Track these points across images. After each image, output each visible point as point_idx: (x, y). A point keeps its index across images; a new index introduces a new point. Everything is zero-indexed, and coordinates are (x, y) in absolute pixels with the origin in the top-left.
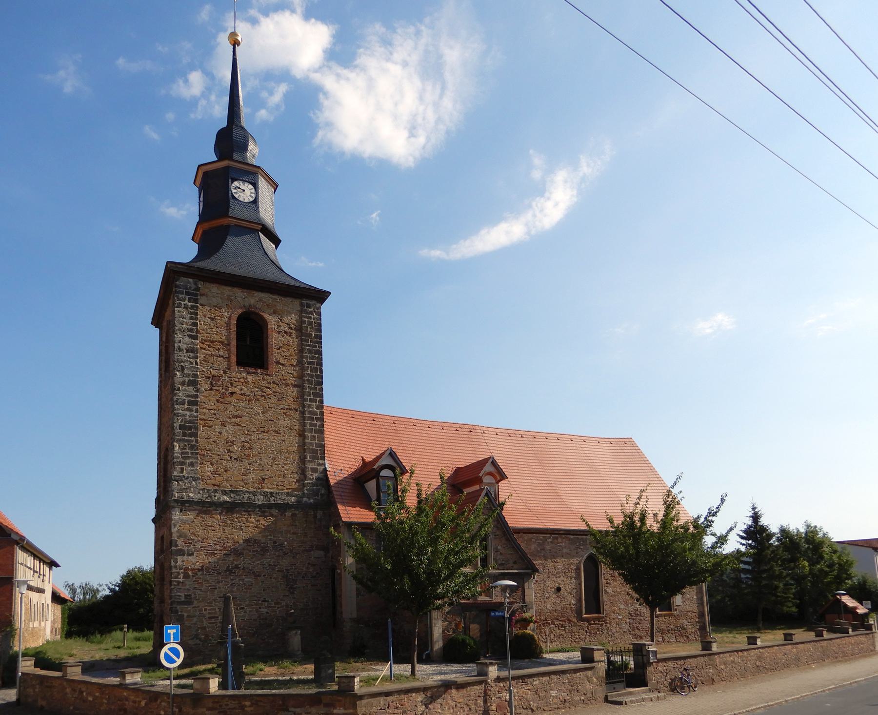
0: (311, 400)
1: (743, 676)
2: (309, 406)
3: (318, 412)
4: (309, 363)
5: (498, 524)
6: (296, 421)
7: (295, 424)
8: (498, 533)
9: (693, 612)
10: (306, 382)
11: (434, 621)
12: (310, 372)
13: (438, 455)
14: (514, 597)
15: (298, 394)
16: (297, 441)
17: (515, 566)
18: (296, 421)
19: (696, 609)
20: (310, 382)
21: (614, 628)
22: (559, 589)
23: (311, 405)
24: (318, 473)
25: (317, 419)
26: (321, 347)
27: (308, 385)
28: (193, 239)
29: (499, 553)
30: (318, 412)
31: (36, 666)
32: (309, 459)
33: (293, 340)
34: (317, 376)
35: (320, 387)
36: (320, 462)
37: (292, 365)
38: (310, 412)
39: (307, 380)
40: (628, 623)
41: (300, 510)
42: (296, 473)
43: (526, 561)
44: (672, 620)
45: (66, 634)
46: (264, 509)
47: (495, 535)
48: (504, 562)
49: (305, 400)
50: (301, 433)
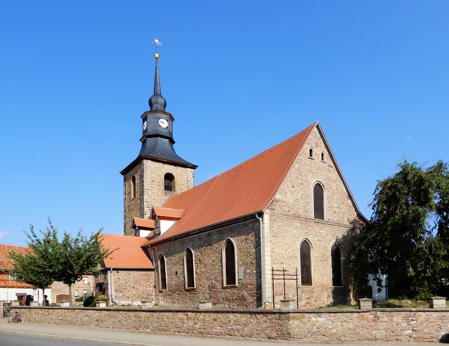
1: (49, 323)
9: (252, 285)
13: (190, 197)
19: (255, 283)
21: (201, 296)
22: (177, 273)
28: (140, 140)
31: (359, 300)
40: (208, 293)
44: (235, 291)
45: (373, 279)
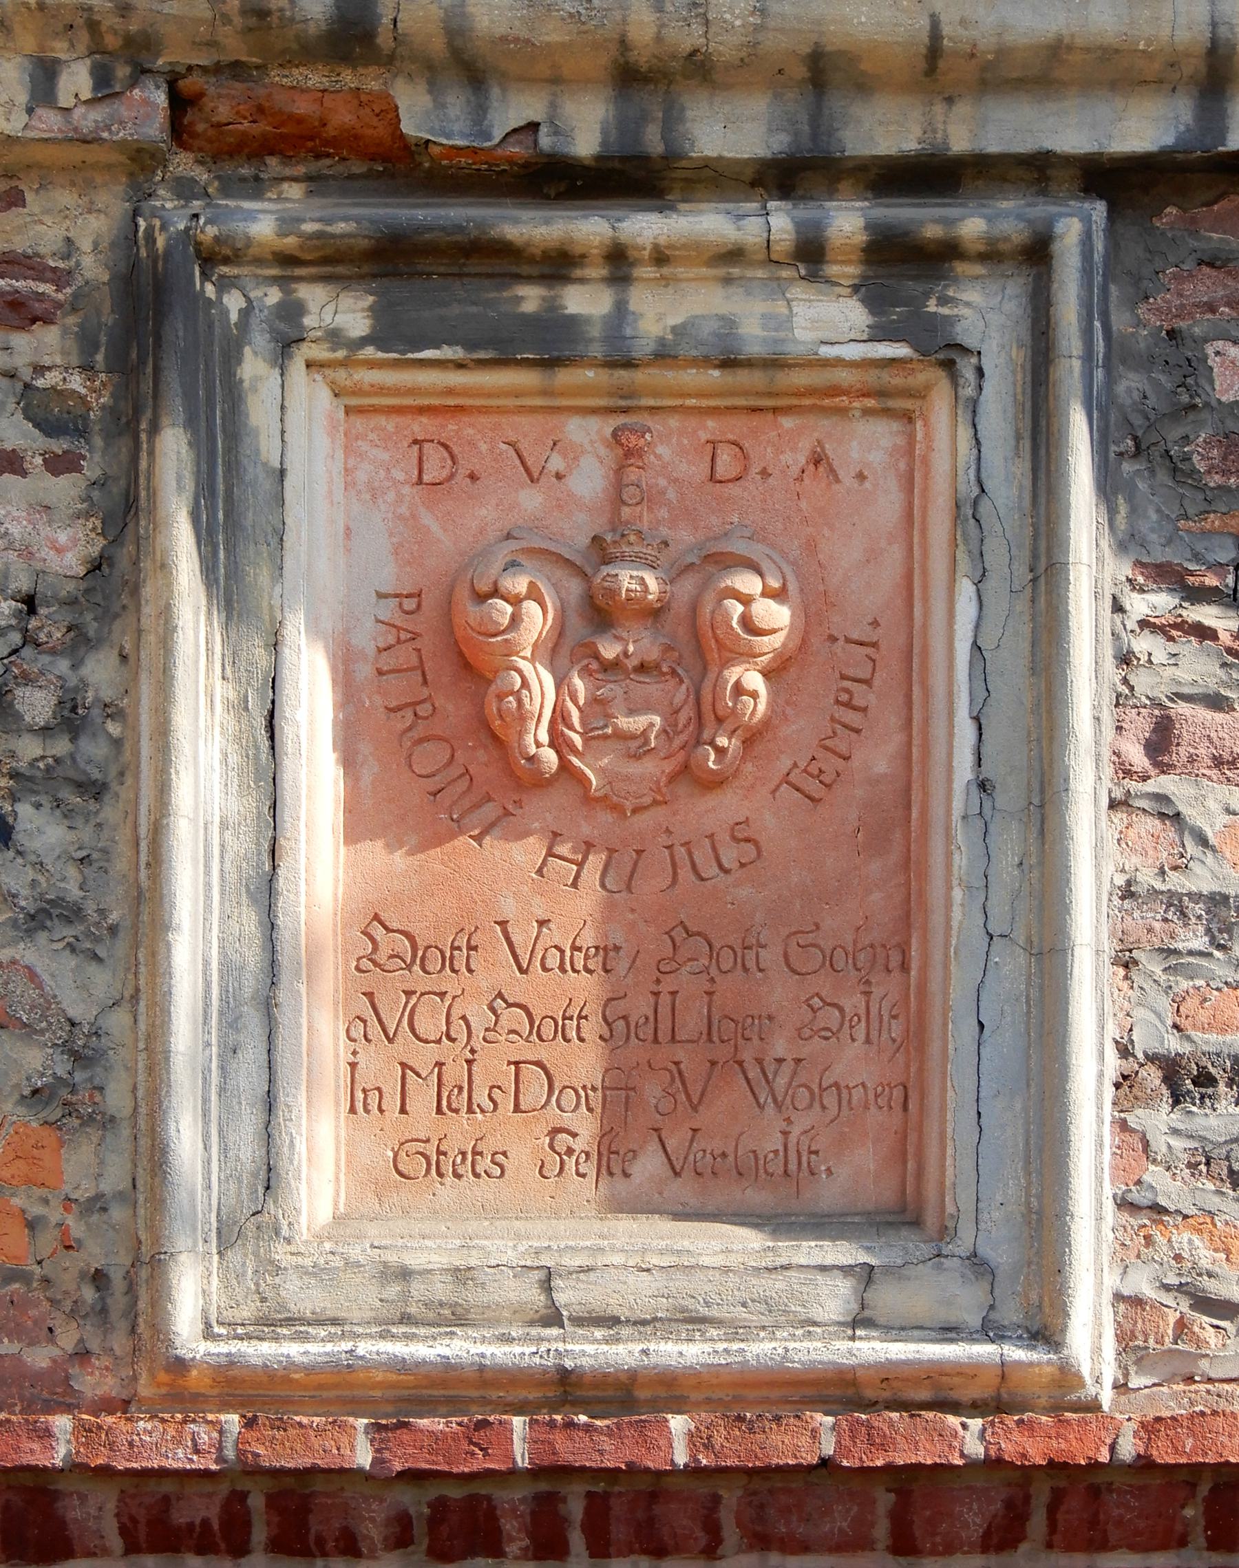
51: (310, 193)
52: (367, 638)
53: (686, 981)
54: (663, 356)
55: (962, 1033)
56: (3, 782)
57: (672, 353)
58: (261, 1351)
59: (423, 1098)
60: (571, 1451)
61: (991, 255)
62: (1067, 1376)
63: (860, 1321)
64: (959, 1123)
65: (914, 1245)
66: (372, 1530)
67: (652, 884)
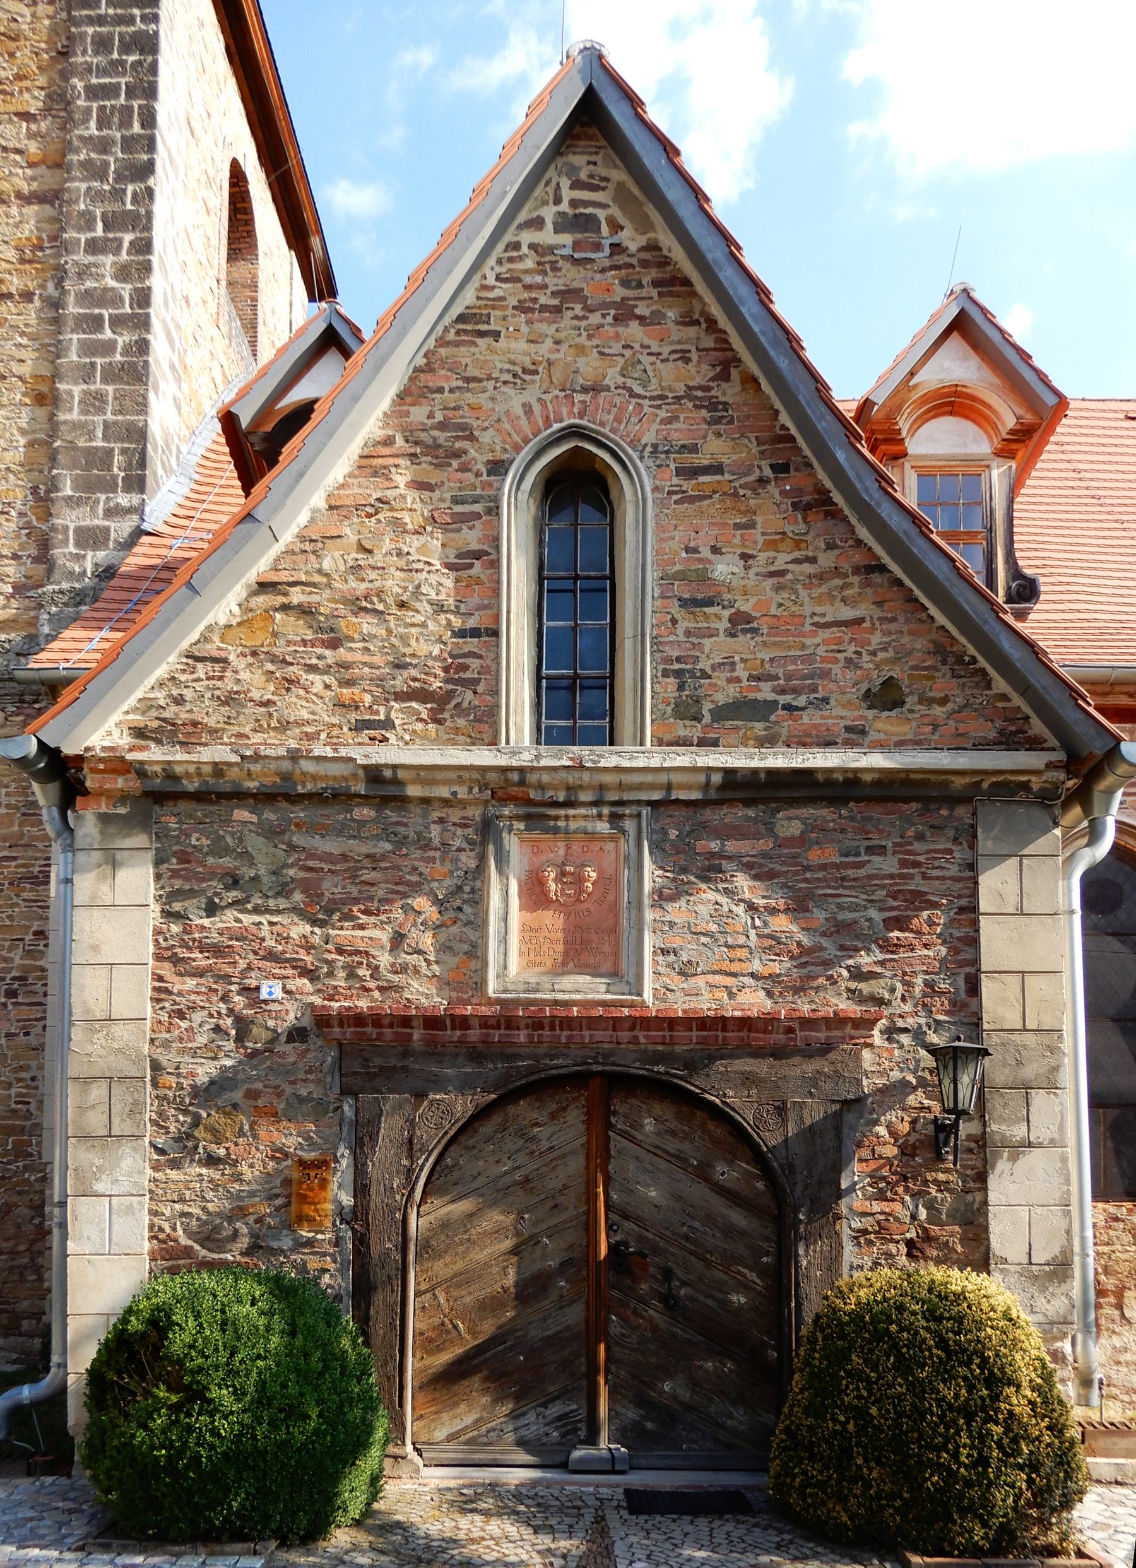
0: (94, 247)
2: (83, 272)
3: (126, 290)
4: (93, 92)
5: (724, 376)
6: (24, 341)
7: (22, 354)
8: (715, 449)
10: (77, 173)
11: (79, 1156)
12: (99, 128)
14: (865, 987)
15: (38, 229)
16: (23, 423)
17: (884, 724)
18: (24, 341)
20: (98, 172)
23: (96, 266)
24: (107, 547)
25: (117, 322)
26: (155, 18)
27: (83, 186)
29: (722, 621)
30: (126, 290)
32: (69, 492)
33: (33, 15)
34: (129, 144)
35: (139, 186)
36: (123, 499)
37: (26, 116)
38: (86, 297)
39: (83, 165)
41: (11, 709)
42: (15, 557)
43: (1000, 684)
46: (1119, 1105)
47: (683, 472)
48: (765, 692)
49: (67, 247)
50: (44, 389)
51: (528, 829)
52: (523, 878)
53: (578, 935)
54: (575, 832)
55: (625, 944)
56: (3, 811)
57: (617, 1142)
58: (503, 996)
59: (532, 953)
60: (556, 1013)
61: (631, 816)
62: (643, 1002)
63: (607, 992)
64: (625, 959)
65: (617, 979)
66: (522, 1026)
67: (572, 918)
